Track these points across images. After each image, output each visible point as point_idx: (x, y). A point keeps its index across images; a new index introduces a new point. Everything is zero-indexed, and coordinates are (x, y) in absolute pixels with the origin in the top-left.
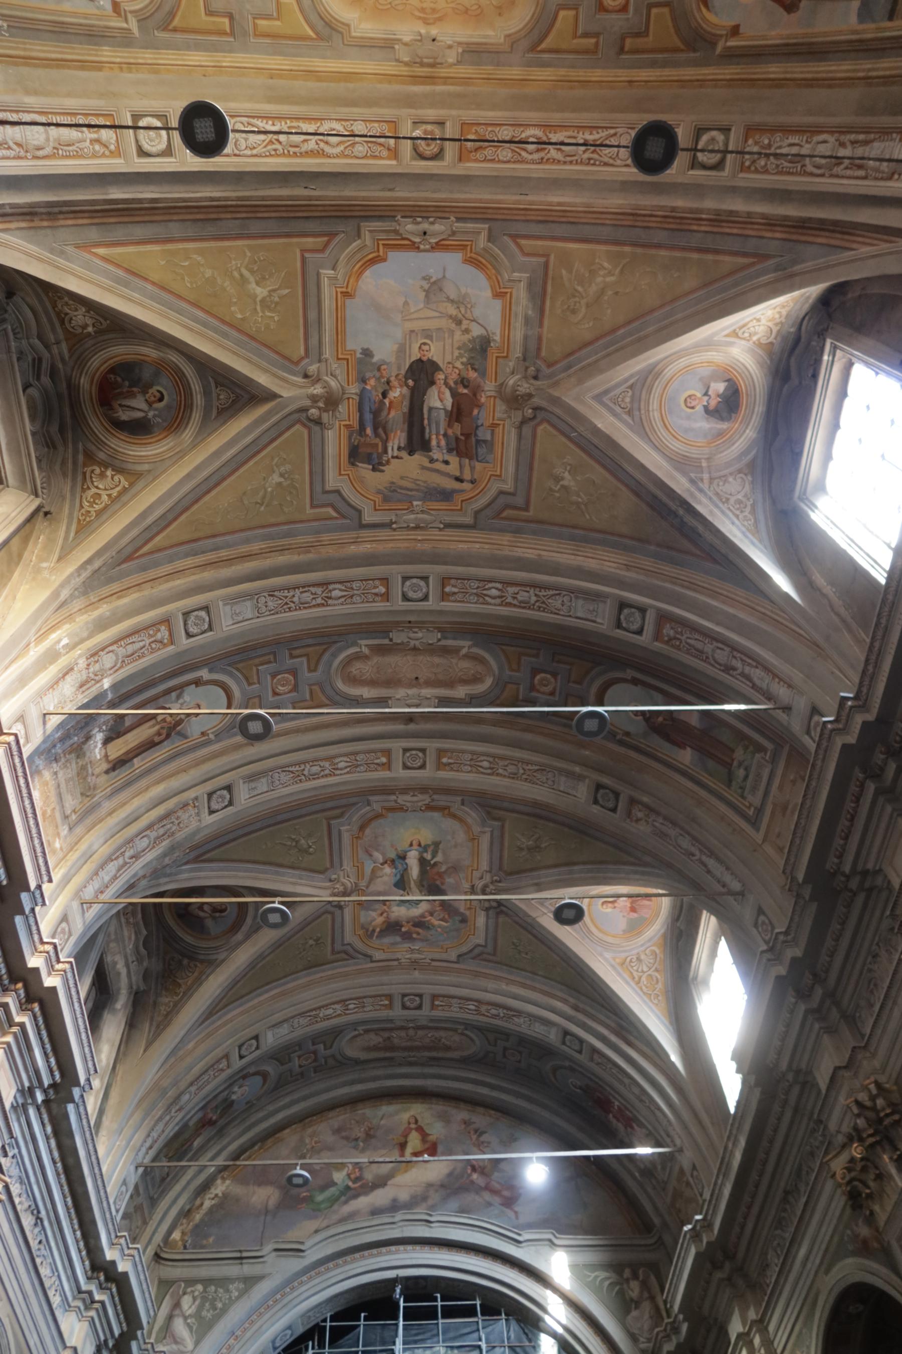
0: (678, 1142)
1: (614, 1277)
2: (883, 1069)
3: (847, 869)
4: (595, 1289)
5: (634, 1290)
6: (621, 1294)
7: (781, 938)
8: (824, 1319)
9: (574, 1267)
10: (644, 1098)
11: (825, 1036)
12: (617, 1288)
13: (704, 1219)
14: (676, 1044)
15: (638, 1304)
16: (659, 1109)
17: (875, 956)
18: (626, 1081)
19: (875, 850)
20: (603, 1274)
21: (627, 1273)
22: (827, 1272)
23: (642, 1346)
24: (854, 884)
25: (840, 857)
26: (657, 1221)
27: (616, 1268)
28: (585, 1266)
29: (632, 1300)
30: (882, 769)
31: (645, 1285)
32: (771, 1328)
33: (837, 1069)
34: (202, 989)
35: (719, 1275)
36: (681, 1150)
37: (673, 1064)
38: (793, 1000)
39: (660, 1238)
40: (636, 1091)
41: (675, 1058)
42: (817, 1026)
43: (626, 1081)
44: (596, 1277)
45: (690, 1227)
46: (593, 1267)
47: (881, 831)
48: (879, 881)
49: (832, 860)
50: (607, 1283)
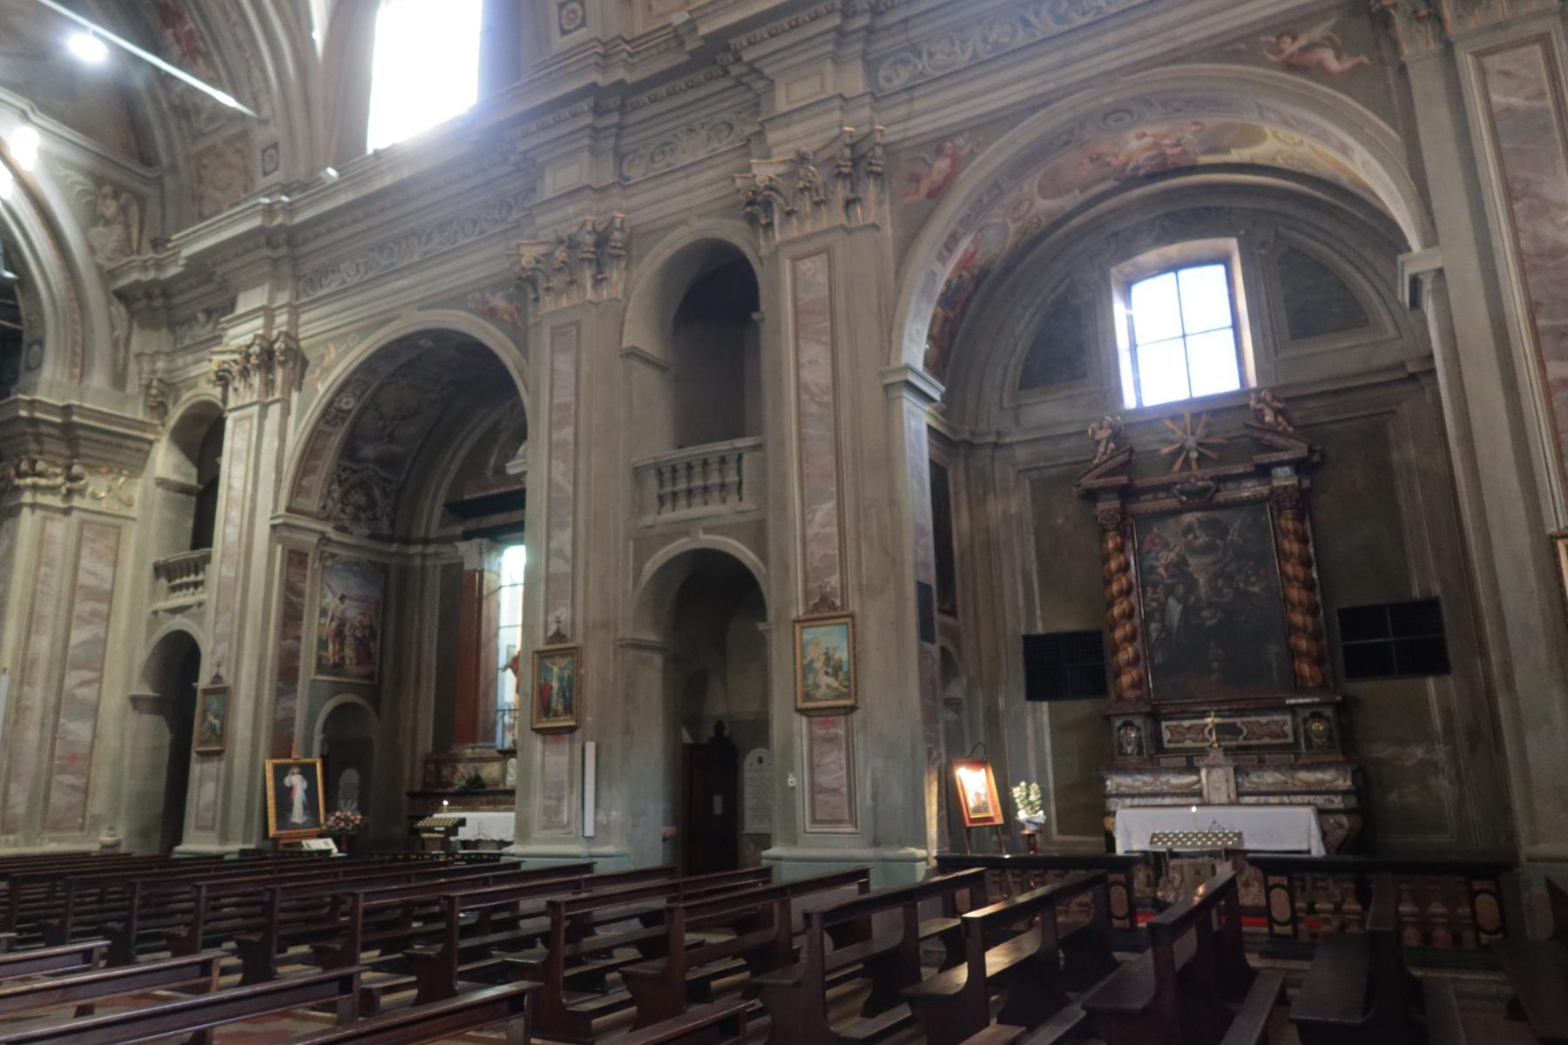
0: (266, 113)
1: (90, 186)
2: (628, 211)
3: (747, 56)
4: (65, 188)
5: (110, 208)
6: (92, 206)
7: (624, 55)
8: (388, 339)
9: (44, 154)
10: (246, 47)
11: (586, 153)
12: (89, 198)
13: (290, 204)
14: (326, 22)
15: (108, 222)
16: (263, 69)
17: (692, 130)
18: (234, 17)
19: (784, 64)
20: (77, 177)
21: (107, 189)
22: (420, 309)
23: (101, 261)
24: (735, 70)
25: (751, 44)
26: (165, 160)
27: (99, 180)
28: (59, 159)
29: (103, 216)
30: (855, 14)
31: (123, 209)
32: (304, 318)
33: (588, 187)
34: (1481, 292)
35: (265, 252)
36: (265, 122)
37: (312, 42)
38: (586, 108)
39: (161, 177)
40: (241, 34)
41: (318, 35)
42: (586, 142)
43: (234, 17)
44: (67, 176)
45: (267, 201)
46: (69, 165)
47: (805, 56)
48: (759, 85)
49: (742, 40)
50: (79, 188)
